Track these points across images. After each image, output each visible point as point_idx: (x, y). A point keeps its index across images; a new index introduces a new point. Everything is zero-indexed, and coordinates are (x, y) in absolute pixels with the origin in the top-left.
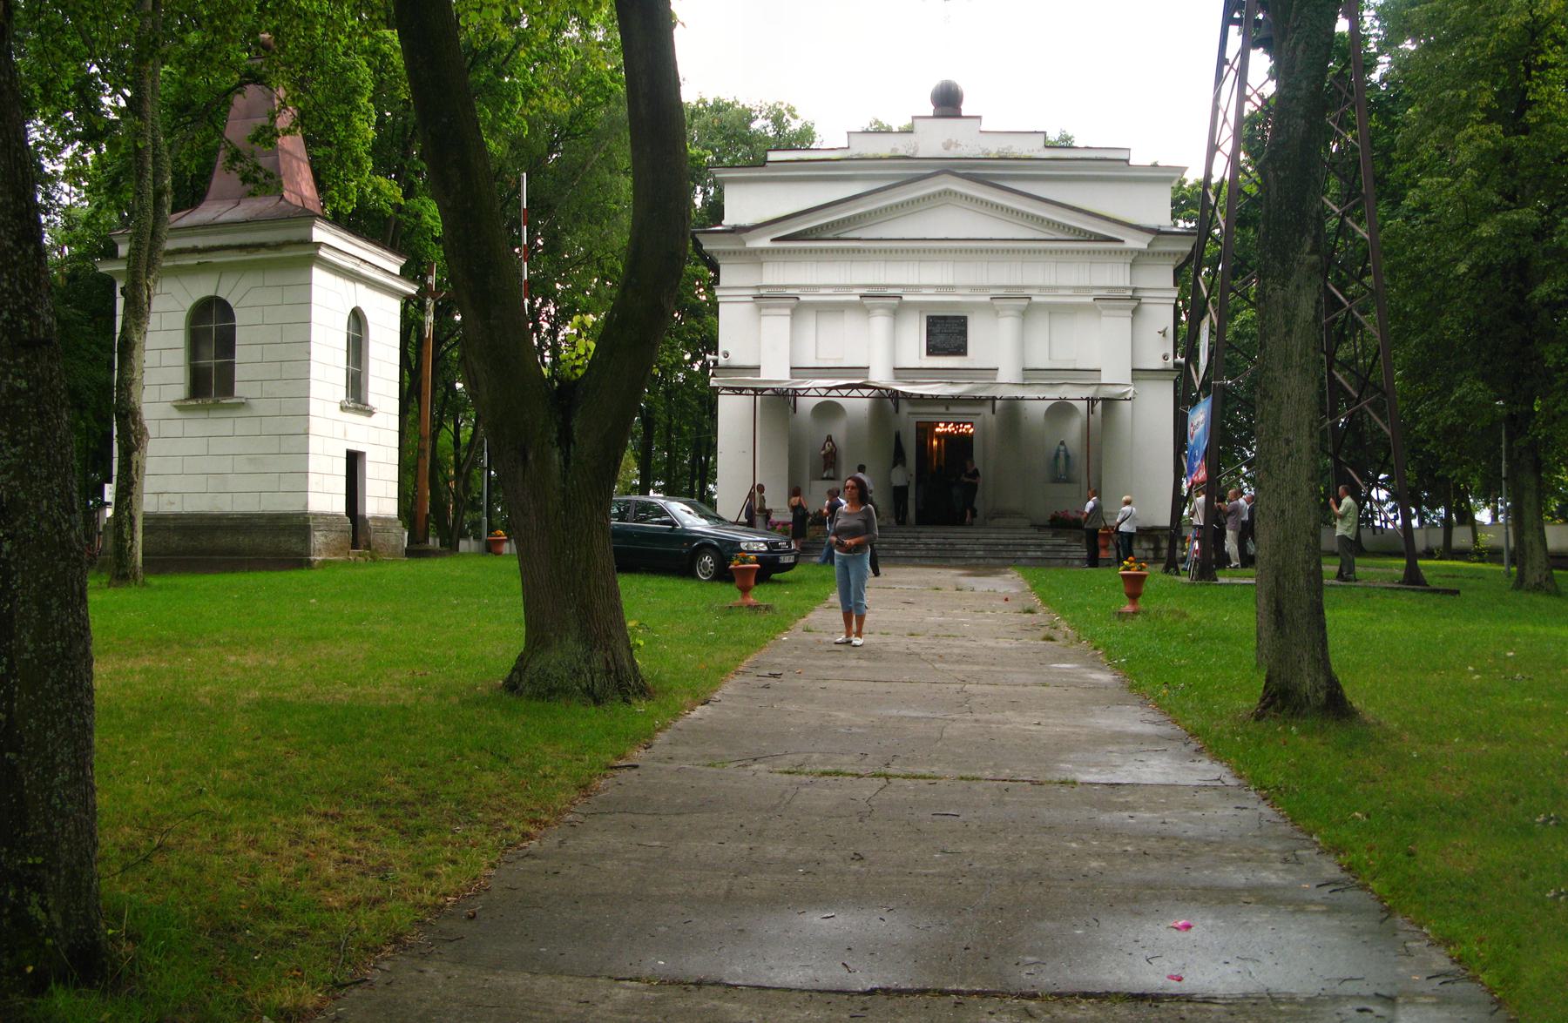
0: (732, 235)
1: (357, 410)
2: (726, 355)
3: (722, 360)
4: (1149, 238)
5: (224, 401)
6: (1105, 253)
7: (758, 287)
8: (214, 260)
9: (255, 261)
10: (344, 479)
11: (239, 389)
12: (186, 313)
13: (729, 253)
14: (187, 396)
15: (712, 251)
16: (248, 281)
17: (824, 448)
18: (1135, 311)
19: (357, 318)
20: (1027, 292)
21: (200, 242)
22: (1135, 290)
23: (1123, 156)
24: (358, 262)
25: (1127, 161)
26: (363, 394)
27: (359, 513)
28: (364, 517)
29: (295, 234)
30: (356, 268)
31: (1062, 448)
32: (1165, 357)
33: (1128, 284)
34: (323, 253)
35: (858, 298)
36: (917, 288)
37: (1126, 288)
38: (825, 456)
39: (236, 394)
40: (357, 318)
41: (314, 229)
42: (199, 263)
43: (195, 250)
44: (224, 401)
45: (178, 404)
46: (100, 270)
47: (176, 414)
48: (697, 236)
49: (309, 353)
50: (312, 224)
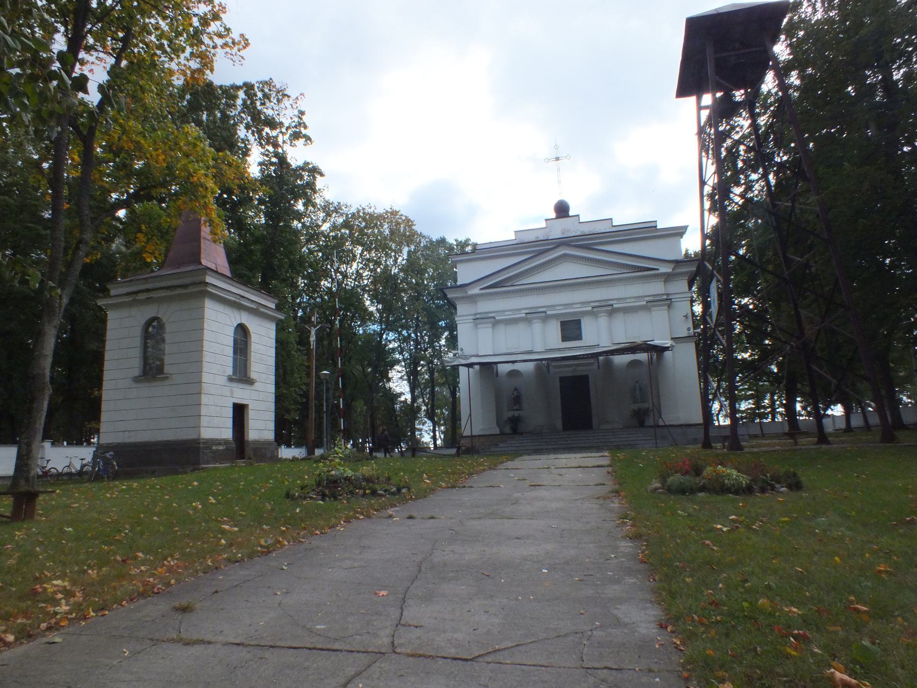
2: (462, 350)
4: (672, 265)
7: (476, 314)
8: (155, 296)
15: (453, 298)
17: (513, 394)
18: (669, 306)
19: (242, 331)
20: (611, 302)
21: (150, 286)
22: (668, 295)
23: (653, 225)
24: (238, 297)
25: (656, 227)
27: (246, 439)
28: (248, 441)
29: (197, 279)
31: (637, 384)
32: (689, 329)
33: (664, 292)
35: (525, 315)
36: (552, 307)
37: (663, 294)
38: (514, 398)
40: (242, 331)
42: (147, 298)
43: (148, 290)
50: (205, 274)
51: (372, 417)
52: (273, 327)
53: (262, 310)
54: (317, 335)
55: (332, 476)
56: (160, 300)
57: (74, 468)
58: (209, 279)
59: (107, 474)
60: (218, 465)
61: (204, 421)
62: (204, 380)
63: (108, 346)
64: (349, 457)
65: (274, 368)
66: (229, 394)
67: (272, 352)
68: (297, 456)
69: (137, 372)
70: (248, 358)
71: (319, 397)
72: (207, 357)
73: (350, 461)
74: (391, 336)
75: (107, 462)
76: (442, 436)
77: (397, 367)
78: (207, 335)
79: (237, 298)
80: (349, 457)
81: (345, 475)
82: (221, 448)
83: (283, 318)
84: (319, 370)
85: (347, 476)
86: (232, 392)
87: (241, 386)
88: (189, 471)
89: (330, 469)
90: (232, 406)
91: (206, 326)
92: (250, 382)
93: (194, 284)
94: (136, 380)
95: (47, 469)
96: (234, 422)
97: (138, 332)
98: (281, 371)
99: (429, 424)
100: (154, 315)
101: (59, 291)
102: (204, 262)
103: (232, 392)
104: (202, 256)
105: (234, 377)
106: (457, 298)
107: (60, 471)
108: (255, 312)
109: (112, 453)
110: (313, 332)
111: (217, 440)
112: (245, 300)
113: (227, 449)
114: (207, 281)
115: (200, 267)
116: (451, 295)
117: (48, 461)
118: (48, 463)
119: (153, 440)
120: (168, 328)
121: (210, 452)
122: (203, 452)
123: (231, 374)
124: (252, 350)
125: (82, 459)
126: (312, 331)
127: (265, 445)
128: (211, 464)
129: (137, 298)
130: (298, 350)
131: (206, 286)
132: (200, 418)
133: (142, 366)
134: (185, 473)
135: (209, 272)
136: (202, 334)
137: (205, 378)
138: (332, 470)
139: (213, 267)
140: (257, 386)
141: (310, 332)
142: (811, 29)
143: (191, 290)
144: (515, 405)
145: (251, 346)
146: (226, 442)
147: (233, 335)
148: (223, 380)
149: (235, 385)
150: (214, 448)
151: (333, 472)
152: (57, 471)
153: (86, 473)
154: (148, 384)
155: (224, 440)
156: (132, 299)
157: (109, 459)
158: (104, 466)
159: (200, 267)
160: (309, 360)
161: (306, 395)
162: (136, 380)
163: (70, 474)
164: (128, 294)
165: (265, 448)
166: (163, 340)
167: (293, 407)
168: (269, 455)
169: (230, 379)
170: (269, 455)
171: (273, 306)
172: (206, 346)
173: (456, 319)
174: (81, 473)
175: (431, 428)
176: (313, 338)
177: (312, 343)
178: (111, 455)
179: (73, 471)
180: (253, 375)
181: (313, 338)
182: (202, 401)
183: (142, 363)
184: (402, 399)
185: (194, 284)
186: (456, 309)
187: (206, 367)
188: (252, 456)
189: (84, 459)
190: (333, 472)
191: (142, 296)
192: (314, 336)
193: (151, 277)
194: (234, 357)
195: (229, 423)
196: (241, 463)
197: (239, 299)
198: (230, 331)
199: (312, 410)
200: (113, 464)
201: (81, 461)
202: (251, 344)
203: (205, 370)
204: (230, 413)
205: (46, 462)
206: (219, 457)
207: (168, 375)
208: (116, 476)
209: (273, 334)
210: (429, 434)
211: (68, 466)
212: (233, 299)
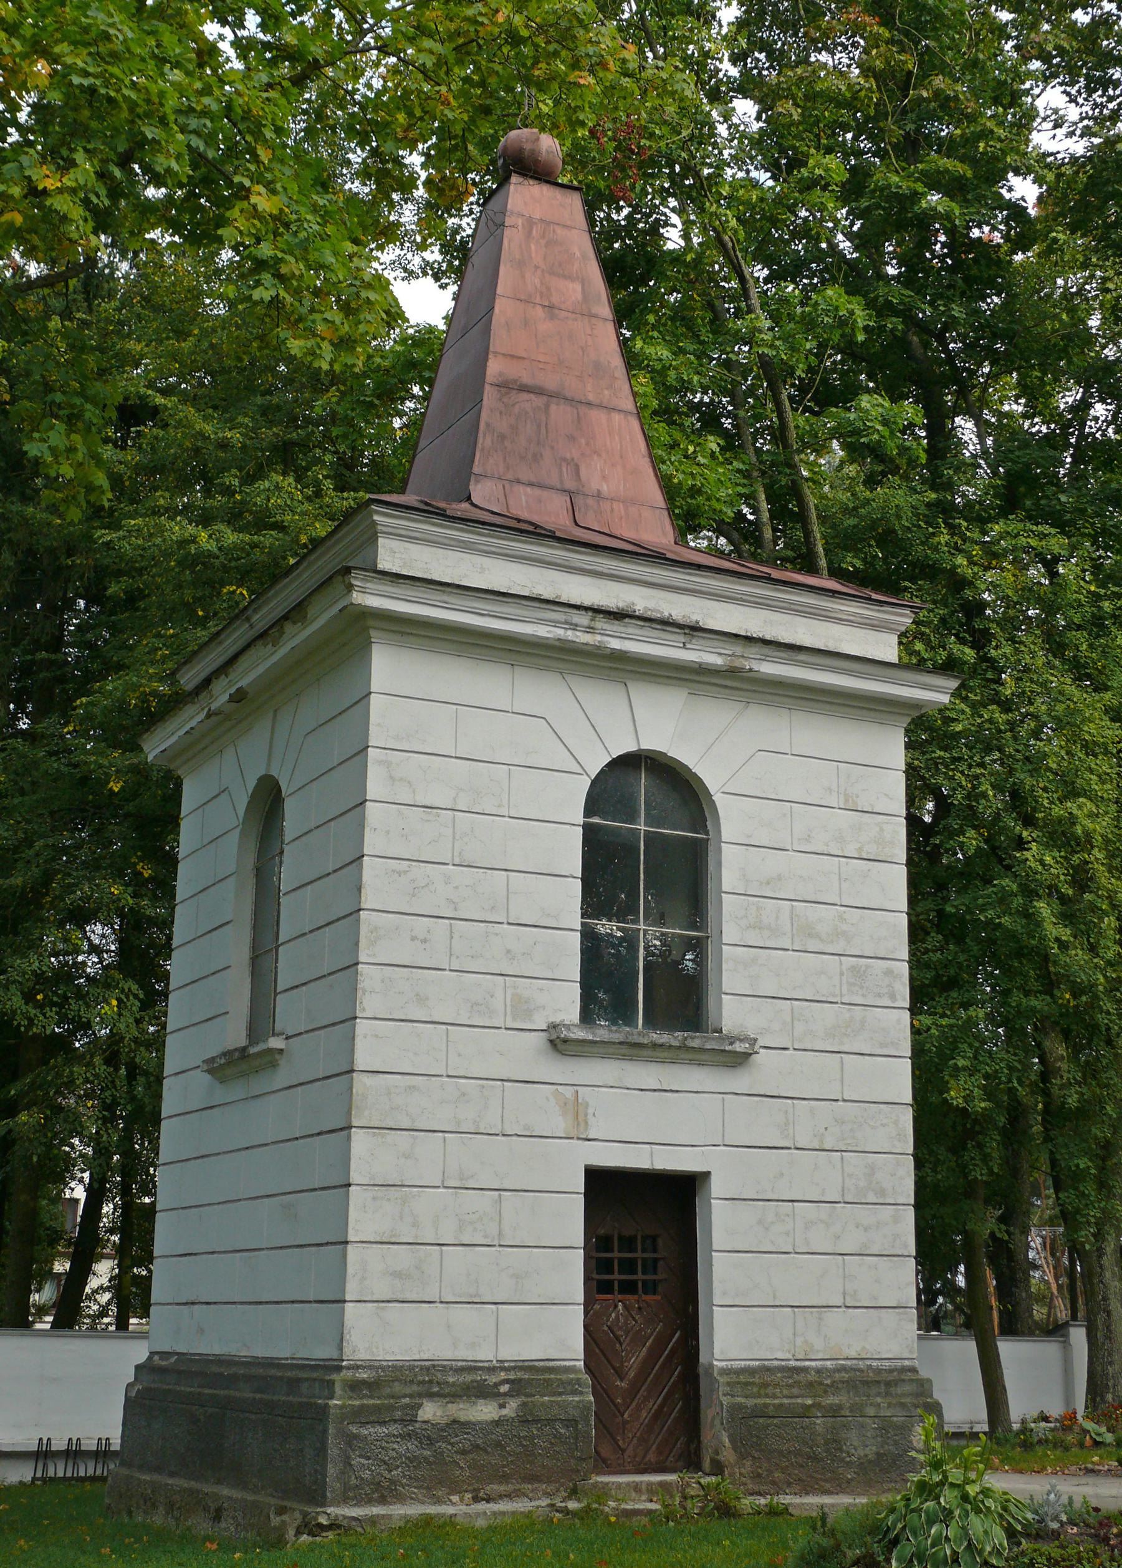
24: (583, 619)
27: (703, 1359)
30: (583, 638)
47: (221, 1094)
60: (455, 1507)
62: (362, 1060)
66: (559, 1124)
79: (574, 627)
82: (484, 1411)
83: (945, 699)
90: (579, 1183)
101: (981, 56)
103: (577, 1112)
112: (631, 628)
113: (525, 1418)
122: (351, 1440)
128: (401, 1499)
142: (969, 197)
144: (281, 1051)
147: (580, 819)
150: (430, 1411)
165: (834, 1412)
171: (887, 649)
188: (728, 1455)
197: (590, 630)
212: (543, 631)
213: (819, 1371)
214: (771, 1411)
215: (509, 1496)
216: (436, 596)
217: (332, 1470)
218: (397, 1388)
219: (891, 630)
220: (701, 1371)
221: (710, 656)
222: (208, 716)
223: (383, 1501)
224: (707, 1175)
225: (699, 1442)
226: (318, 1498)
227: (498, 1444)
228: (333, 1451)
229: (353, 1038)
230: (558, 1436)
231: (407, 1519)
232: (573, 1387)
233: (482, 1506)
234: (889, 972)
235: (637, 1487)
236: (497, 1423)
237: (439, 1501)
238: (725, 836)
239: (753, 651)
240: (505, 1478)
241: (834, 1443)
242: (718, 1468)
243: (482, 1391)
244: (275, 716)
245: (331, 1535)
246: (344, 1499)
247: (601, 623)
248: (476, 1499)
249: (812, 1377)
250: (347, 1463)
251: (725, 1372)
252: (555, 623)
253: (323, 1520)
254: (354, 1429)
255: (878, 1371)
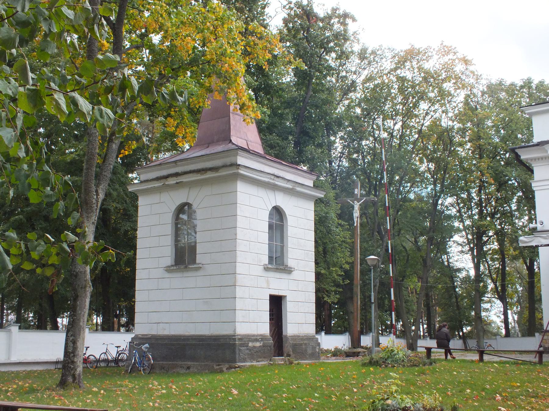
0: (538, 147)
1: (277, 270)
2: (542, 223)
3: (539, 227)
5: (190, 267)
6: (539, 159)
8: (184, 180)
9: (219, 177)
10: (136, 311)
11: (199, 258)
12: (172, 213)
13: (539, 159)
14: (173, 264)
15: (527, 159)
16: (206, 191)
19: (278, 212)
21: (179, 169)
24: (273, 177)
26: (285, 260)
27: (284, 333)
28: (286, 336)
29: (228, 161)
30: (272, 181)
34: (242, 171)
39: (197, 261)
40: (278, 212)
41: (238, 157)
42: (177, 183)
43: (177, 175)
44: (190, 267)
45: (166, 269)
46: (130, 190)
47: (167, 275)
48: (517, 151)
49: (236, 234)
50: (237, 155)
51: (427, 295)
52: (311, 206)
53: (299, 189)
54: (361, 209)
55: (388, 405)
56: (191, 185)
57: (111, 355)
58: (242, 160)
59: (143, 367)
60: (255, 363)
61: (239, 316)
63: (140, 254)
64: (403, 361)
65: (314, 253)
66: (265, 285)
67: (311, 236)
68: (340, 347)
69: (169, 260)
70: (285, 244)
71: (365, 285)
72: (241, 246)
73: (404, 366)
74: (450, 200)
75: (143, 355)
76: (516, 317)
77: (456, 238)
78: (241, 222)
79: (271, 179)
80: (403, 361)
81: (403, 406)
82: (258, 344)
83: (323, 196)
84: (365, 253)
85: (406, 407)
86: (268, 282)
87: (278, 275)
88: (224, 369)
89: (386, 396)
91: (239, 213)
92: (288, 270)
93: (225, 166)
94: (168, 269)
95: (87, 356)
96: (271, 315)
97: (169, 218)
98: (321, 249)
99: (498, 305)
100: (184, 201)
102: (233, 139)
103: (268, 282)
104: (232, 133)
105: (270, 266)
106: (535, 159)
107: (98, 357)
108: (291, 192)
109: (147, 345)
110: (357, 206)
111: (254, 336)
112: (279, 180)
113: (264, 346)
114: (239, 163)
115: (230, 146)
116: (524, 156)
117: (87, 348)
118: (87, 350)
119: (187, 334)
120: (199, 214)
121: (247, 349)
122: (240, 350)
123: (267, 262)
124: (289, 234)
125: (118, 347)
126: (355, 206)
127: (304, 340)
128: (247, 362)
129: (166, 183)
130: (340, 225)
131: (239, 168)
132: (235, 313)
133: (174, 233)
134: (221, 371)
135: (240, 152)
136: (236, 221)
137: (240, 268)
138: (388, 399)
139: (244, 145)
140: (295, 275)
141: (353, 207)
143: (224, 172)
145: (287, 230)
146: (263, 338)
147: (268, 220)
148: (259, 270)
149: (271, 274)
150: (250, 344)
151: (389, 402)
152: (95, 357)
153: (122, 360)
154: (179, 275)
155: (261, 335)
156: (162, 184)
157: (145, 352)
158: (140, 358)
159: (230, 146)
160: (353, 236)
161: (348, 275)
162: (168, 269)
163: (106, 361)
164: (158, 179)
165: (306, 344)
166: (195, 227)
167: (333, 289)
168: (309, 351)
169: (266, 269)
170: (309, 351)
172: (240, 234)
173: (533, 185)
174: (116, 361)
175: (502, 309)
176: (356, 214)
177: (355, 220)
178: (146, 348)
179: (110, 358)
180: (291, 263)
181: (356, 214)
182: (237, 271)
183: (174, 229)
184: (463, 275)
185: (225, 166)
186: (532, 171)
187: (240, 257)
188: (291, 353)
189: (120, 347)
190: (389, 402)
191: (172, 181)
192: (358, 212)
193: (181, 160)
194: (269, 244)
195: (266, 316)
196: (279, 360)
198: (265, 216)
199: (357, 296)
200: (149, 358)
201: (117, 348)
202: (287, 228)
203: (239, 259)
204: (266, 305)
205: (85, 349)
206: (255, 354)
207: (200, 266)
208: (152, 370)
209: (311, 216)
210: (498, 316)
211: (105, 353)
212: (266, 180)
213: (302, 336)
214: (297, 344)
215: (261, 361)
216: (251, 171)
217: (237, 356)
218: (245, 340)
219: (312, 180)
220: (283, 337)
221: (289, 186)
222: (163, 185)
223: (244, 362)
224: (286, 296)
225: (283, 351)
226: (235, 362)
227: (260, 351)
228: (237, 352)
229: (236, 267)
230: (268, 349)
231: (249, 365)
232: (269, 340)
233: (258, 363)
234: (312, 254)
235: (279, 359)
236: (260, 346)
237: (252, 362)
238: (289, 224)
239: (297, 185)
240: (261, 358)
241: (306, 350)
242: (289, 355)
243: (257, 340)
244: (190, 189)
245: (238, 369)
246: (239, 362)
247: (276, 179)
248: (257, 362)
249: (301, 337)
250: (239, 354)
251: (289, 336)
252: (268, 178)
253: (237, 366)
254: (240, 348)
255: (310, 336)
